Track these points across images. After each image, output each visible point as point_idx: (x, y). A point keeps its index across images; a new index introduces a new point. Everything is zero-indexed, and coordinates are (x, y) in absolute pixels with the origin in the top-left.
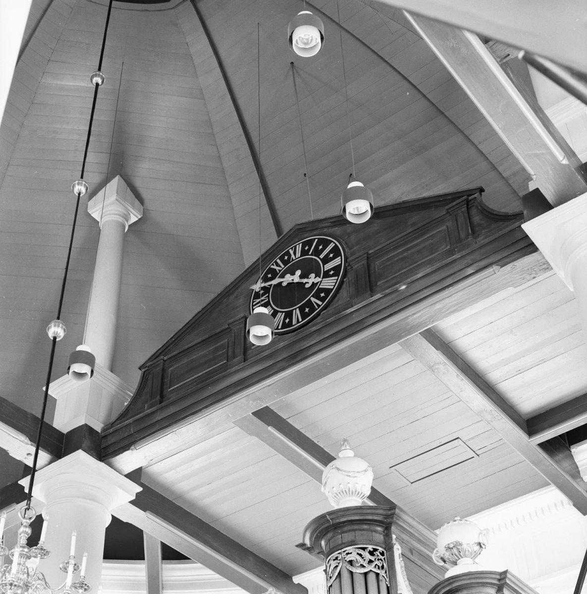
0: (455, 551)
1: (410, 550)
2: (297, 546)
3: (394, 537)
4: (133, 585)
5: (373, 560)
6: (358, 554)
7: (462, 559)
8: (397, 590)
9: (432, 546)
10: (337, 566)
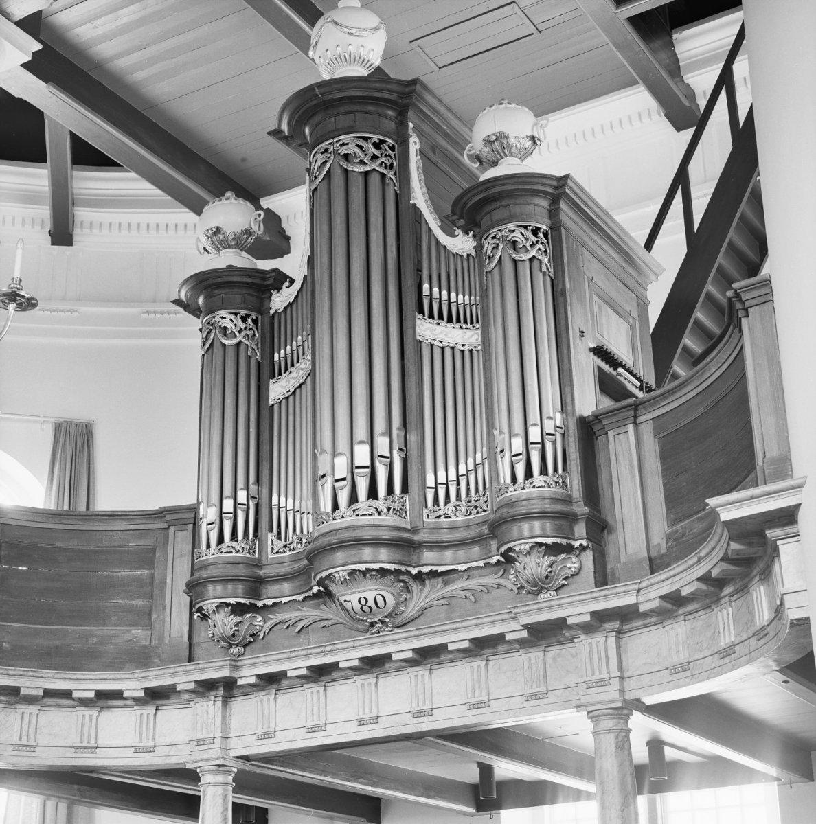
0: (497, 144)
1: (432, 147)
2: (269, 133)
3: (411, 125)
4: (29, 198)
5: (379, 155)
6: (357, 145)
7: (505, 159)
8: (409, 199)
9: (460, 143)
10: (325, 162)
